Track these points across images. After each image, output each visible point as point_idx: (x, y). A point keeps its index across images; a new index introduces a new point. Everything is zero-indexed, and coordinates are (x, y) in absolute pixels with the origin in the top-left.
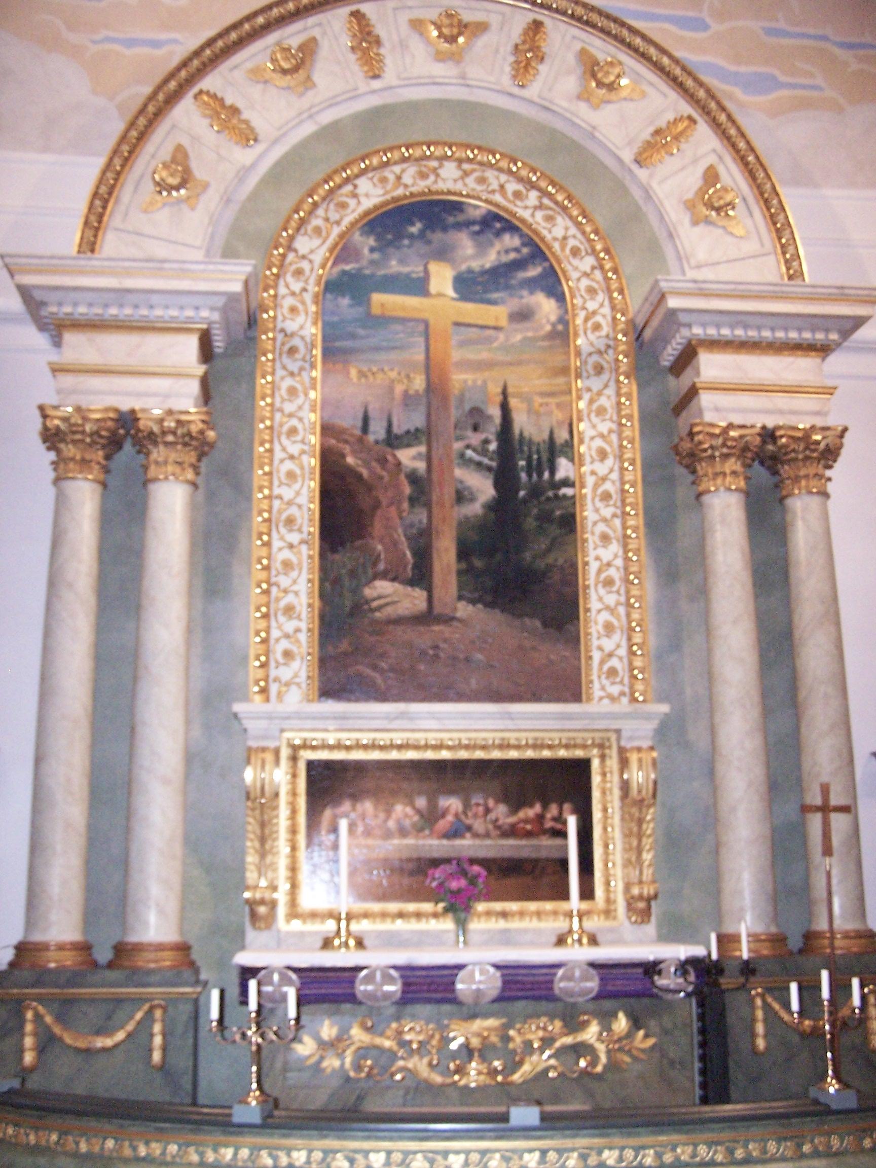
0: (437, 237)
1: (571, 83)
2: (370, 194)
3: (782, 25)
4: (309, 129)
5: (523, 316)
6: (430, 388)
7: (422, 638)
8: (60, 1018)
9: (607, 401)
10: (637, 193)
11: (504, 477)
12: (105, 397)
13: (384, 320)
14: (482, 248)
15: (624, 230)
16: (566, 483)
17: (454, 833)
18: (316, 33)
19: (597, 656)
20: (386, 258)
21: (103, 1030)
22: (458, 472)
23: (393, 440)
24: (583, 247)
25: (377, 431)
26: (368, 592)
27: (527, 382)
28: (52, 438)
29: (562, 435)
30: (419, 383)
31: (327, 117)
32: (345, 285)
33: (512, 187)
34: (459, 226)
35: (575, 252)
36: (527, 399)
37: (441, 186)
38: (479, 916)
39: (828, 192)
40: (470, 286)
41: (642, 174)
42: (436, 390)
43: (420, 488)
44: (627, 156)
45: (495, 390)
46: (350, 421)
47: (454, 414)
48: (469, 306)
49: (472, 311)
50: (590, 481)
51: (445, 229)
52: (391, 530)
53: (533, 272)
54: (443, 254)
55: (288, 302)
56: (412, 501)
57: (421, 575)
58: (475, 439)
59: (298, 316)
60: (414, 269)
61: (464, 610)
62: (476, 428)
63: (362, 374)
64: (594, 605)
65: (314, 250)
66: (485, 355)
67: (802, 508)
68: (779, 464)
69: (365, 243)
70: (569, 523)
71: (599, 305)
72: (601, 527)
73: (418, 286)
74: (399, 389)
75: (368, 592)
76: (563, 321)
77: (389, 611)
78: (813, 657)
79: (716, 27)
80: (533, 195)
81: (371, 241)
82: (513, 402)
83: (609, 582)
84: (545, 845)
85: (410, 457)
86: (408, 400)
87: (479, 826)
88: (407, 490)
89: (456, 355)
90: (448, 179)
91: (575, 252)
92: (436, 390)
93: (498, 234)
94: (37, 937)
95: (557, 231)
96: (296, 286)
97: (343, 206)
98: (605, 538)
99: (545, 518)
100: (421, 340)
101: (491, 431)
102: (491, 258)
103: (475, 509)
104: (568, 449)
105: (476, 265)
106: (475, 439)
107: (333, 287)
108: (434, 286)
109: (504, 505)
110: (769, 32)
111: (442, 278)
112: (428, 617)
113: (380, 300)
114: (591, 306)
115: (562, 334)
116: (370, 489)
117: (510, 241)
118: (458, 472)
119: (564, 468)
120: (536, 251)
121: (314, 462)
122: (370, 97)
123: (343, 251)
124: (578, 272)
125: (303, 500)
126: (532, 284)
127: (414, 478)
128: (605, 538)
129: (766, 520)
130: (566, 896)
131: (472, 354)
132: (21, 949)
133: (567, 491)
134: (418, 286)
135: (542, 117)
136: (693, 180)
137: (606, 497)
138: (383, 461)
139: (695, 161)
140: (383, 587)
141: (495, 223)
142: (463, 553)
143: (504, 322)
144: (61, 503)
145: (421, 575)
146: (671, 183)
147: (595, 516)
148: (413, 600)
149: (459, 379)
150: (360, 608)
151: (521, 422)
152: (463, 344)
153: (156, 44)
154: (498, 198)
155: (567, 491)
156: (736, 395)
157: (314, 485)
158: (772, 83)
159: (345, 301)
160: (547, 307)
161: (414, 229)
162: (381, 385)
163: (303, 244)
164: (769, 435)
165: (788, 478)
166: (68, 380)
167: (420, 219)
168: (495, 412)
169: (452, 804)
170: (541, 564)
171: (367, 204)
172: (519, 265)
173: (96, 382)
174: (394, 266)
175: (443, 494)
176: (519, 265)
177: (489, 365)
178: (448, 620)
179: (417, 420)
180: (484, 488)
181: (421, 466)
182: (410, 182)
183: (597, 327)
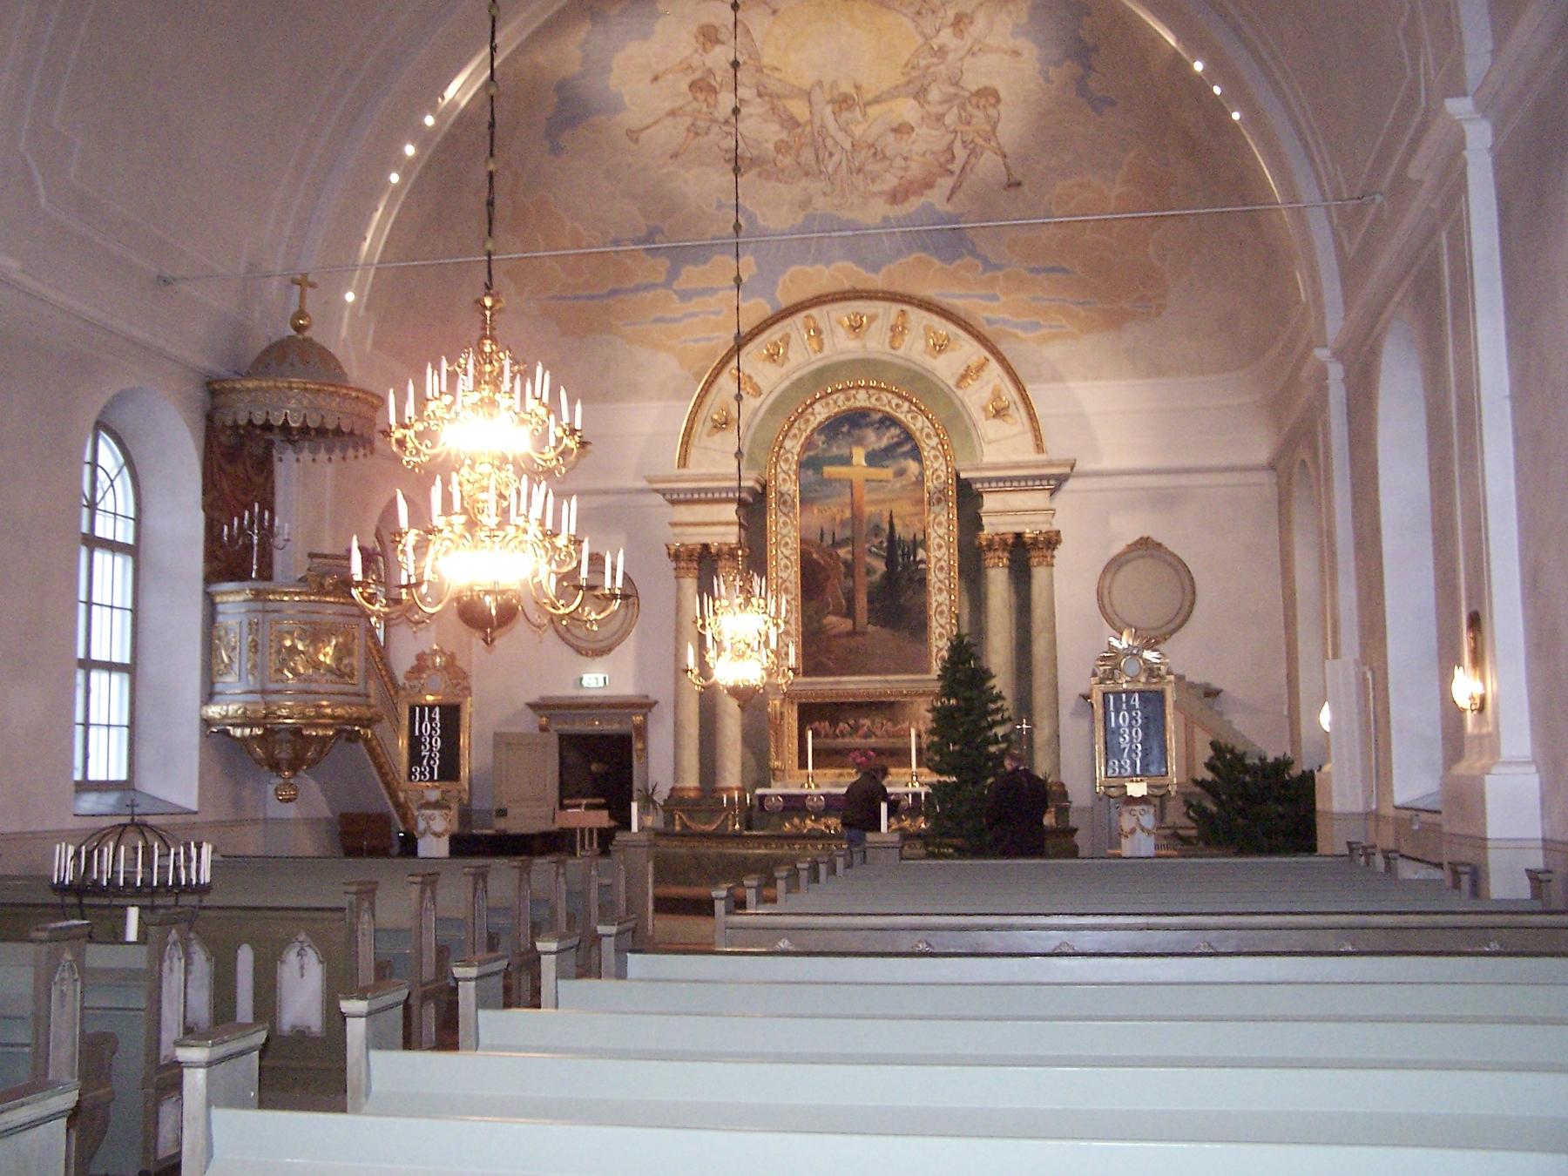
0: (856, 432)
1: (920, 345)
2: (821, 413)
3: (1040, 294)
4: (786, 383)
5: (901, 473)
6: (854, 516)
7: (853, 642)
8: (690, 817)
9: (943, 518)
10: (958, 403)
11: (890, 561)
12: (695, 537)
13: (829, 482)
14: (879, 438)
15: (954, 425)
16: (922, 561)
17: (866, 736)
18: (788, 330)
19: (935, 650)
20: (830, 447)
21: (709, 823)
22: (868, 559)
23: (836, 544)
24: (932, 433)
25: (828, 540)
26: (825, 622)
27: (903, 509)
28: (676, 556)
29: (920, 537)
30: (848, 514)
31: (795, 376)
32: (811, 463)
33: (895, 401)
34: (867, 425)
35: (928, 436)
36: (901, 518)
37: (858, 404)
38: (1057, 767)
39: (1071, 384)
40: (874, 459)
41: (959, 393)
42: (856, 517)
43: (850, 567)
44: (952, 383)
45: (886, 514)
46: (815, 537)
47: (865, 529)
48: (873, 470)
49: (875, 473)
50: (933, 561)
51: (860, 427)
52: (835, 590)
53: (906, 448)
54: (860, 442)
55: (781, 476)
56: (846, 576)
57: (850, 613)
58: (876, 541)
59: (788, 484)
60: (845, 451)
61: (870, 628)
62: (876, 535)
63: (820, 511)
64: (934, 624)
65: (793, 446)
66: (881, 496)
67: (1039, 574)
68: (1024, 554)
69: (820, 440)
70: (923, 582)
71: (940, 464)
72: (938, 585)
73: (847, 461)
74: (838, 518)
75: (825, 622)
76: (922, 474)
77: (835, 631)
78: (1039, 648)
79: (1003, 299)
80: (906, 405)
81: (823, 438)
82: (896, 521)
83: (942, 613)
84: (899, 743)
85: (843, 553)
86: (843, 523)
87: (879, 733)
88: (843, 569)
89: (866, 498)
90: (861, 400)
91: (928, 436)
92: (856, 517)
93: (888, 428)
94: (679, 785)
95: (918, 425)
96: (785, 467)
97: (807, 421)
98: (940, 590)
99: (910, 579)
100: (848, 491)
101: (884, 538)
102: (884, 442)
103: (876, 577)
104: (923, 544)
105: (876, 447)
106: (876, 541)
107: (802, 465)
108: (855, 460)
109: (891, 577)
110: (1034, 299)
111: (859, 456)
112: (852, 633)
113: (829, 470)
114: (936, 465)
115: (920, 481)
116: (823, 568)
117: (895, 431)
118: (868, 559)
119: (921, 554)
120: (908, 436)
121: (796, 558)
122: (818, 361)
123: (808, 444)
124: (929, 447)
125: (792, 577)
126: (905, 455)
127: (845, 563)
128: (940, 590)
129: (1021, 576)
130: (806, 767)
131: (873, 496)
132: (672, 790)
133: (922, 566)
134: (847, 461)
135: (907, 364)
136: (986, 394)
137: (942, 568)
138: (831, 556)
139: (988, 383)
140: (832, 619)
141: (889, 421)
142: (870, 601)
143: (891, 477)
144: (679, 589)
145: (850, 613)
146: (975, 397)
147: (935, 578)
148: (846, 625)
149: (869, 510)
150: (821, 630)
151: (899, 530)
152: (870, 491)
153: (709, 339)
154: (887, 409)
155: (922, 566)
156: (1003, 514)
157: (797, 568)
158: (1037, 326)
159: (810, 472)
160: (913, 466)
161: (845, 429)
162: (830, 514)
163: (788, 444)
164: (1019, 536)
165: (438, 835)
166: (678, 530)
167: (851, 422)
168: (886, 526)
169: (866, 722)
170: (908, 604)
171: (820, 418)
172: (899, 445)
173: (691, 530)
174: (835, 451)
175: (860, 571)
176: (899, 445)
177: (883, 501)
178: (863, 634)
179: (848, 533)
180: (880, 566)
181: (849, 557)
182: (840, 404)
183: (938, 477)
